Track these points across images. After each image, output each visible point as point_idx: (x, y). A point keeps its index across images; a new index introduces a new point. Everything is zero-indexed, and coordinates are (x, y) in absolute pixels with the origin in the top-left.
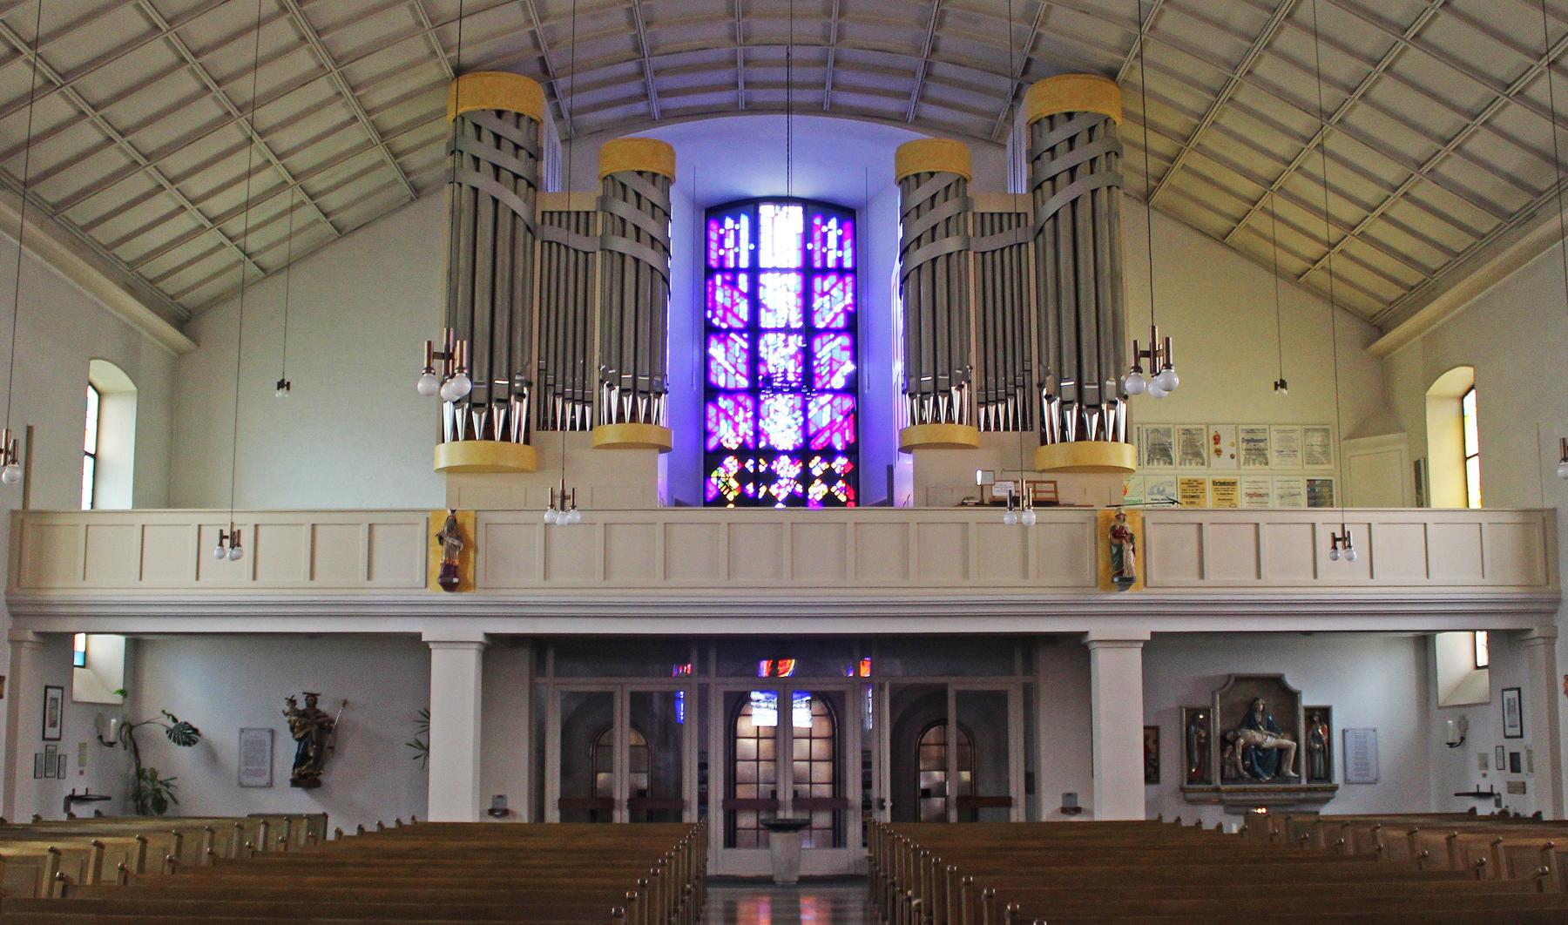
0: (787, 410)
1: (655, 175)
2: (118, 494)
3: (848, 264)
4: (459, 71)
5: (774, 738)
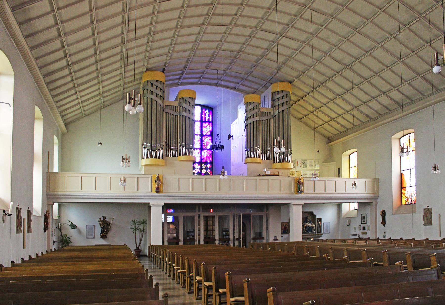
3: (211, 120)
4: (147, 70)
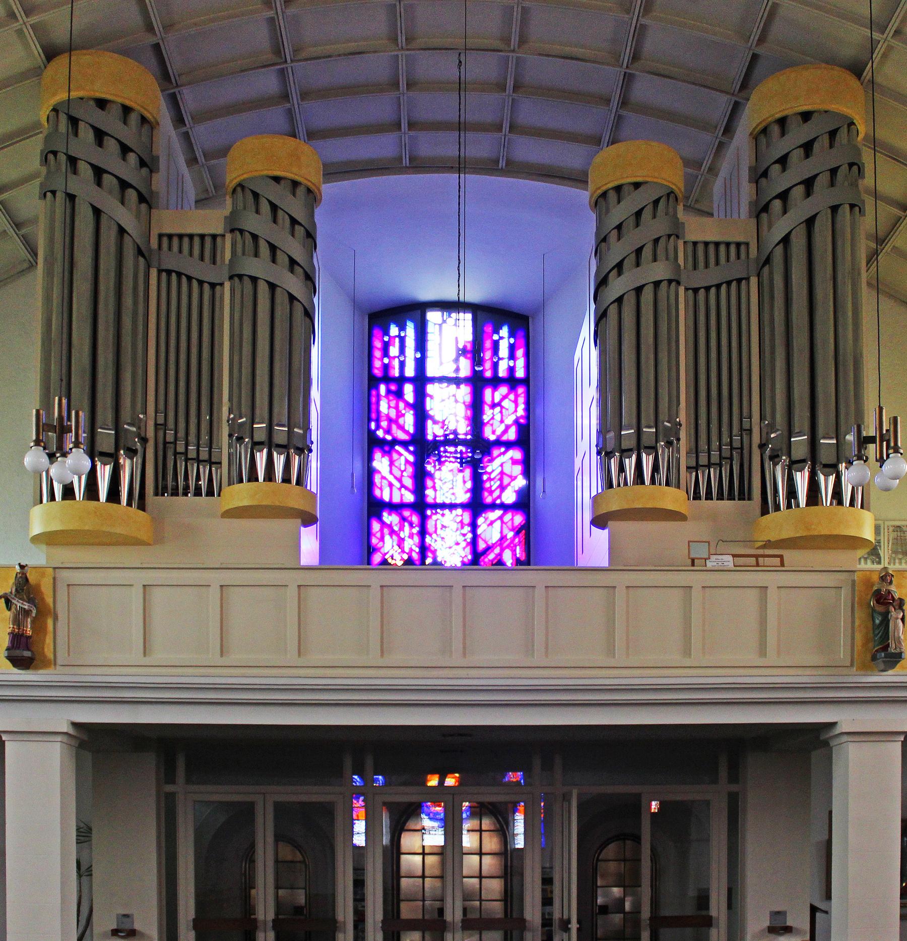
0: (455, 526)
1: (295, 184)
3: (520, 373)
5: (441, 877)
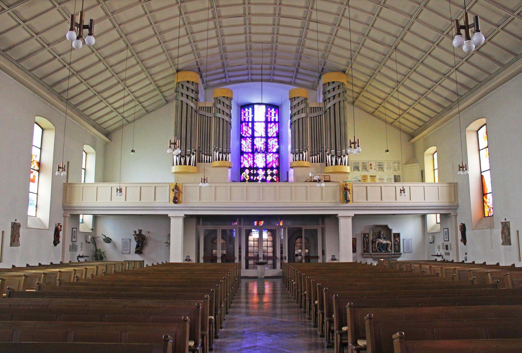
2: (91, 178)
3: (277, 120)
4: (178, 71)
